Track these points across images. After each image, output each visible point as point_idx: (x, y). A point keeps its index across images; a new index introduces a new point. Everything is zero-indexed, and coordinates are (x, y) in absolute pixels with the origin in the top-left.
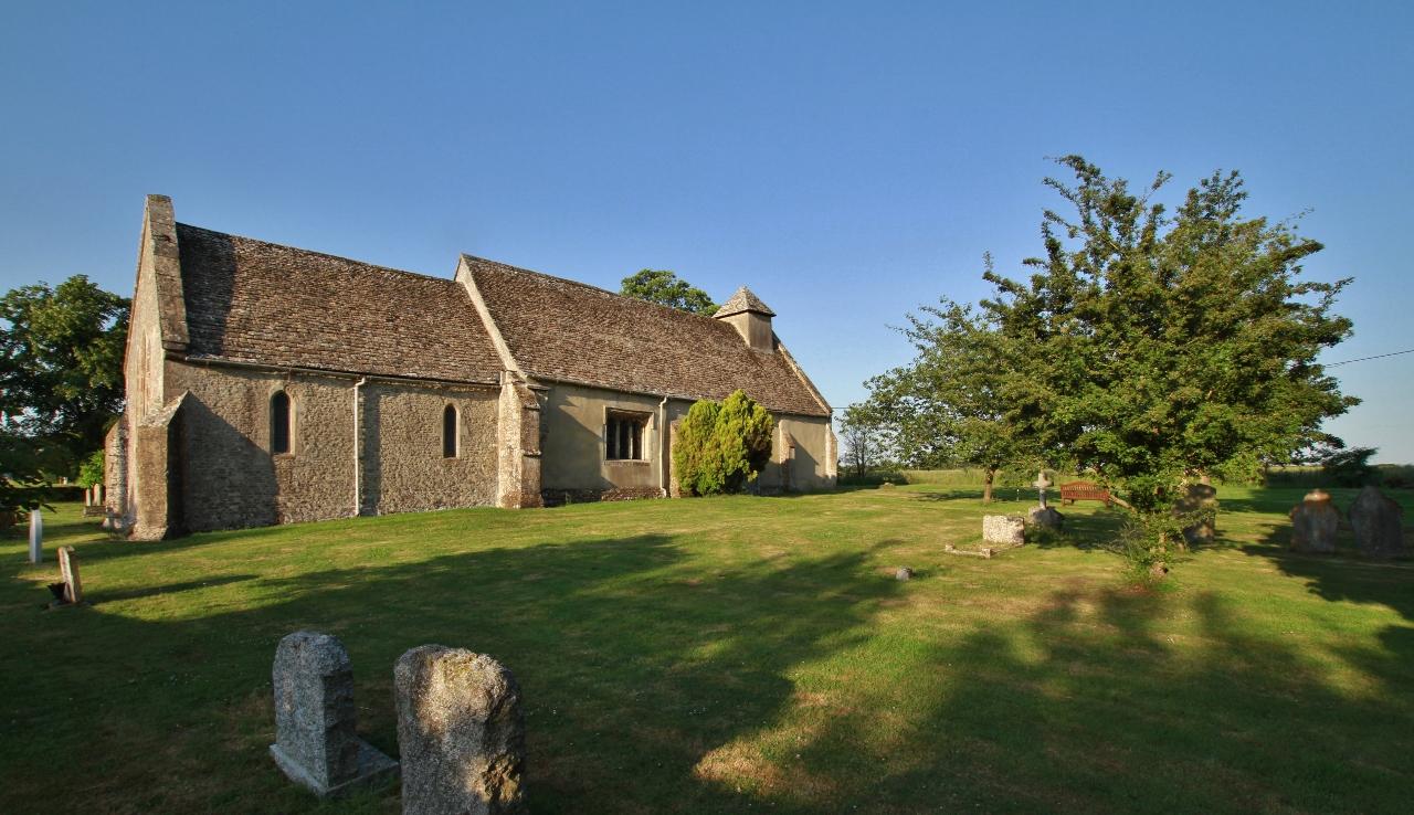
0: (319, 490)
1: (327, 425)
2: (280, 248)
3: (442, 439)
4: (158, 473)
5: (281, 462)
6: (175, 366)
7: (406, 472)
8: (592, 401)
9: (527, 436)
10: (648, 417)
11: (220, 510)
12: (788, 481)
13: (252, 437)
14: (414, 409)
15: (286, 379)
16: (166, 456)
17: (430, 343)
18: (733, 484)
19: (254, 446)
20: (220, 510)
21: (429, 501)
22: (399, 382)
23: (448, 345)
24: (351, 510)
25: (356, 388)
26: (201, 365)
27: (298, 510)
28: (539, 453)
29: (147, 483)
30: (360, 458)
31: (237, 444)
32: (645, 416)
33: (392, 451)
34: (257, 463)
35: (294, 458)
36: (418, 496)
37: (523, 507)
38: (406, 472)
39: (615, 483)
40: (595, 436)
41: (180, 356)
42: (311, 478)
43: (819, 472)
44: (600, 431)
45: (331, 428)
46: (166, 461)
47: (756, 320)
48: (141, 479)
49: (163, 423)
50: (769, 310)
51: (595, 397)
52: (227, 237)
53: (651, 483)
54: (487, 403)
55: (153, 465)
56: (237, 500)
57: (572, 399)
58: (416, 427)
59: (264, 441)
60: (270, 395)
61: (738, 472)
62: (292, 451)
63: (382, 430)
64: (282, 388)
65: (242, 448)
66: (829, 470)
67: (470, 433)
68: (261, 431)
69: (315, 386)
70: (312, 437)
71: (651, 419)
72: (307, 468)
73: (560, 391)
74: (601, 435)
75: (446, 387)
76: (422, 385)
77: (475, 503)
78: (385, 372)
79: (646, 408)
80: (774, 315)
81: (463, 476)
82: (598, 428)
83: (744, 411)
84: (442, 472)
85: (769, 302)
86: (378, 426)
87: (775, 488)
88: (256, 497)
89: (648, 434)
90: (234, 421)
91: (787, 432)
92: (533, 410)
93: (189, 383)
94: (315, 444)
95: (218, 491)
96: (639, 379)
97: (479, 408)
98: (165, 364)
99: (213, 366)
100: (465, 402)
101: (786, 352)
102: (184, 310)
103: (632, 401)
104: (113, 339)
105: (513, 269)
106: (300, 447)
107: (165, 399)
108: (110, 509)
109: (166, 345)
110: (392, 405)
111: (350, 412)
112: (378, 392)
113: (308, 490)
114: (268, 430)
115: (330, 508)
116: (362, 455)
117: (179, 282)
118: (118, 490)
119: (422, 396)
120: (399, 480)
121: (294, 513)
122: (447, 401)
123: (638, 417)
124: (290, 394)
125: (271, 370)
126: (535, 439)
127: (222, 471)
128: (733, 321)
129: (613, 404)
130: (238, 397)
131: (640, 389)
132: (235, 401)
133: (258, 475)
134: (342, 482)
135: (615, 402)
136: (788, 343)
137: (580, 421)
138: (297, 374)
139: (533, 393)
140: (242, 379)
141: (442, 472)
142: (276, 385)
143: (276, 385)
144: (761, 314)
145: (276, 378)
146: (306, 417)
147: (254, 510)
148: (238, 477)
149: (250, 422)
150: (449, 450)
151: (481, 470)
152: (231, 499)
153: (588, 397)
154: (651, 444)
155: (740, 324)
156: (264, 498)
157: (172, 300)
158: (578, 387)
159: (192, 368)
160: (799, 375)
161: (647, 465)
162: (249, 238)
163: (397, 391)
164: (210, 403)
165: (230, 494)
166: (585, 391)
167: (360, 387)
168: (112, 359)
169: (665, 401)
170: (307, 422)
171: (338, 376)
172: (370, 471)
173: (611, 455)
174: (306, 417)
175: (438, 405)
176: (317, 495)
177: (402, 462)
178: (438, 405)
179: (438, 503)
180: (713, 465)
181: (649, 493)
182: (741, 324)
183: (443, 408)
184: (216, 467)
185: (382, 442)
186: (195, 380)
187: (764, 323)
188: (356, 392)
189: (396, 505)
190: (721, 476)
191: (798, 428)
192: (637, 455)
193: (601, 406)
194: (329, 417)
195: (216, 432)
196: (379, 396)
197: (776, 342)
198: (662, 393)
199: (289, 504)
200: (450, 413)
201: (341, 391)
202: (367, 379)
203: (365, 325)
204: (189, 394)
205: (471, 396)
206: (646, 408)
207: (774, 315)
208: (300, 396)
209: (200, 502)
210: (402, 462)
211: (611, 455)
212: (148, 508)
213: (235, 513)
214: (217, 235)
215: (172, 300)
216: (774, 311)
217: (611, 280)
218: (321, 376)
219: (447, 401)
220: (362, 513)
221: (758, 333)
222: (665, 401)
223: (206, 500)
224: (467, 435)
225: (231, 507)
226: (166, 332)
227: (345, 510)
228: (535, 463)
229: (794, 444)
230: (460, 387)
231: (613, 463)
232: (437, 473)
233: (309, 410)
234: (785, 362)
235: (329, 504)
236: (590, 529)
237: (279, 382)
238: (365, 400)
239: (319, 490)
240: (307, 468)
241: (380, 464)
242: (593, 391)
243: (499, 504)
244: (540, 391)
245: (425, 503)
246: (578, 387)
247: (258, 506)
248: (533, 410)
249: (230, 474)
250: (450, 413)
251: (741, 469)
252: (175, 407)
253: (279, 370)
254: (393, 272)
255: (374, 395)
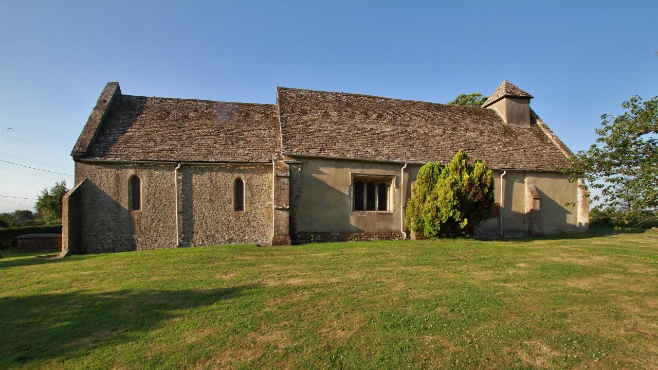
1: (160, 193)
2: (171, 99)
3: (233, 200)
5: (135, 215)
6: (80, 165)
9: (279, 195)
10: (391, 179)
11: (102, 242)
12: (532, 227)
13: (119, 202)
14: (214, 182)
15: (136, 168)
17: (238, 140)
18: (449, 230)
19: (120, 206)
21: (224, 238)
22: (204, 165)
23: (250, 141)
26: (91, 163)
27: (144, 243)
30: (179, 213)
31: (111, 206)
32: (390, 179)
33: (200, 208)
34: (122, 216)
39: (361, 228)
40: (343, 194)
42: (152, 224)
43: (570, 220)
44: (347, 190)
47: (514, 103)
50: (526, 94)
51: (343, 167)
53: (393, 228)
56: (111, 237)
57: (325, 170)
58: (216, 192)
59: (125, 203)
60: (128, 178)
61: (451, 220)
62: (141, 210)
64: (134, 173)
65: (113, 207)
66: (581, 218)
67: (252, 194)
68: (124, 198)
69: (153, 171)
71: (394, 181)
72: (149, 219)
73: (311, 162)
74: (347, 193)
75: (235, 166)
76: (218, 166)
78: (196, 160)
79: (389, 172)
80: (533, 97)
82: (345, 188)
83: (463, 168)
84: (233, 221)
85: (524, 87)
86: (192, 194)
87: (519, 232)
88: (121, 235)
89: (391, 192)
90: (109, 193)
91: (533, 187)
92: (284, 177)
93: (87, 174)
94: (153, 205)
96: (386, 152)
99: (97, 163)
100: (248, 176)
101: (544, 125)
102: (92, 136)
105: (311, 92)
110: (199, 180)
112: (191, 172)
113: (150, 232)
114: (127, 198)
115: (162, 242)
116: (181, 210)
117: (99, 121)
119: (219, 174)
120: (205, 225)
121: (142, 244)
123: (383, 180)
124: (139, 177)
125: (128, 163)
126: (285, 198)
127: (104, 221)
128: (494, 107)
129: (358, 171)
130: (112, 180)
131: (384, 159)
133: (122, 223)
134: (170, 227)
135: (360, 170)
136: (545, 117)
137: (329, 184)
139: (288, 166)
141: (233, 221)
142: (131, 172)
143: (131, 172)
144: (518, 98)
145: (131, 168)
146: (148, 189)
147: (120, 242)
148: (112, 224)
149: (118, 193)
150: (239, 207)
151: (260, 219)
152: (108, 235)
153: (336, 167)
154: (394, 199)
155: (499, 109)
156: (126, 236)
158: (327, 160)
160: (554, 141)
161: (390, 214)
163: (203, 171)
164: (97, 184)
165: (108, 233)
166: (333, 163)
167: (178, 170)
171: (166, 165)
172: (187, 220)
173: (358, 206)
174: (148, 189)
175: (227, 180)
176: (155, 234)
177: (206, 214)
179: (230, 240)
180: (430, 215)
181: (390, 235)
182: (500, 109)
183: (233, 180)
184: (100, 218)
185: (194, 202)
186: (90, 172)
187: (522, 105)
189: (203, 241)
190: (437, 222)
191: (546, 185)
192: (383, 206)
195: (100, 199)
196: (191, 174)
197: (533, 118)
198: (404, 160)
199: (139, 239)
200: (239, 183)
201: (168, 173)
203: (199, 135)
205: (253, 171)
206: (389, 172)
209: (92, 237)
210: (206, 214)
211: (358, 206)
213: (110, 244)
214: (141, 98)
216: (531, 94)
217: (446, 99)
218: (156, 165)
219: (236, 176)
220: (180, 246)
223: (96, 236)
224: (250, 196)
225: (109, 240)
228: (285, 215)
229: (539, 196)
230: (245, 166)
231: (358, 214)
232: (230, 221)
233: (149, 185)
234: (541, 132)
236: (63, 265)
237: (133, 170)
238: (183, 177)
240: (149, 219)
241: (192, 216)
242: (340, 162)
244: (294, 164)
245: (221, 240)
246: (327, 160)
247: (122, 240)
248: (284, 177)
249: (108, 222)
250: (239, 183)
251: (452, 217)
253: (133, 163)
255: (188, 174)
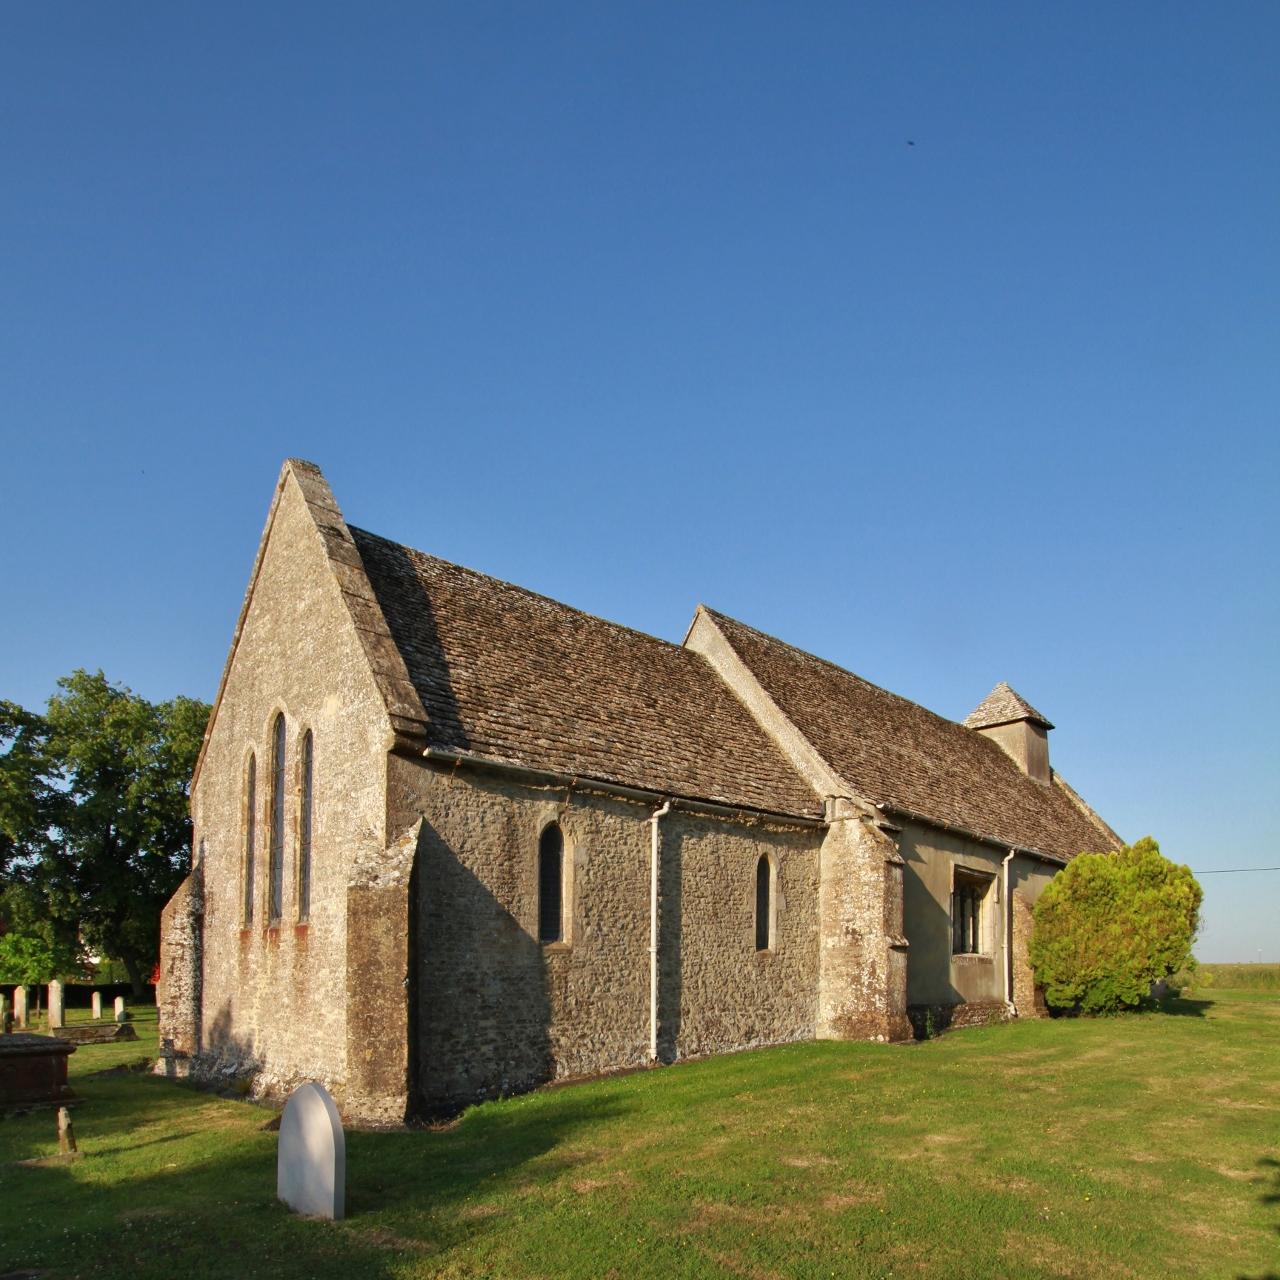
0: (602, 1012)
4: (388, 983)
6: (404, 766)
7: (711, 978)
8: (939, 852)
13: (513, 911)
15: (561, 800)
16: (405, 948)
20: (466, 1055)
24: (645, 1047)
25: (654, 821)
28: (906, 942)
29: (366, 1003)
35: (570, 952)
36: (726, 1021)
37: (892, 1040)
38: (711, 978)
41: (417, 746)
42: (593, 990)
45: (619, 895)
46: (405, 958)
48: (354, 996)
49: (398, 880)
52: (399, 548)
53: (995, 993)
54: (808, 854)
55: (380, 968)
56: (492, 1035)
62: (566, 938)
63: (685, 897)
64: (556, 818)
65: (498, 931)
70: (595, 911)
72: (587, 971)
77: (793, 1032)
80: (1052, 727)
81: (778, 981)
84: (753, 977)
88: (517, 1027)
93: (424, 802)
95: (466, 1016)
97: (799, 860)
98: (391, 768)
100: (782, 851)
103: (978, 856)
104: (18, 769)
106: (578, 928)
107: (389, 833)
108: (169, 1043)
109: (397, 724)
111: (644, 864)
115: (616, 1045)
118: (185, 1007)
119: (732, 839)
120: (702, 991)
122: (763, 847)
127: (471, 977)
132: (491, 839)
138: (580, 792)
140: (501, 799)
141: (753, 977)
143: (546, 811)
148: (494, 990)
149: (510, 880)
150: (762, 942)
156: (530, 1031)
157: (379, 642)
159: (429, 773)
162: (428, 554)
164: (454, 843)
167: (662, 819)
168: (17, 797)
169: (1012, 855)
170: (588, 882)
178: (743, 852)
182: (1012, 742)
183: (758, 858)
188: (655, 827)
193: (947, 862)
194: (617, 872)
196: (679, 837)
198: (1008, 840)
201: (633, 826)
202: (672, 804)
204: (425, 824)
207: (1052, 727)
208: (580, 834)
212: (368, 1054)
215: (379, 642)
221: (1035, 754)
222: (1012, 855)
225: (484, 1049)
226: (390, 698)
227: (635, 1049)
233: (591, 861)
235: (614, 1037)
237: (552, 805)
239: (602, 1012)
240: (587, 971)
243: (825, 1032)
252: (410, 847)
254: (621, 629)
